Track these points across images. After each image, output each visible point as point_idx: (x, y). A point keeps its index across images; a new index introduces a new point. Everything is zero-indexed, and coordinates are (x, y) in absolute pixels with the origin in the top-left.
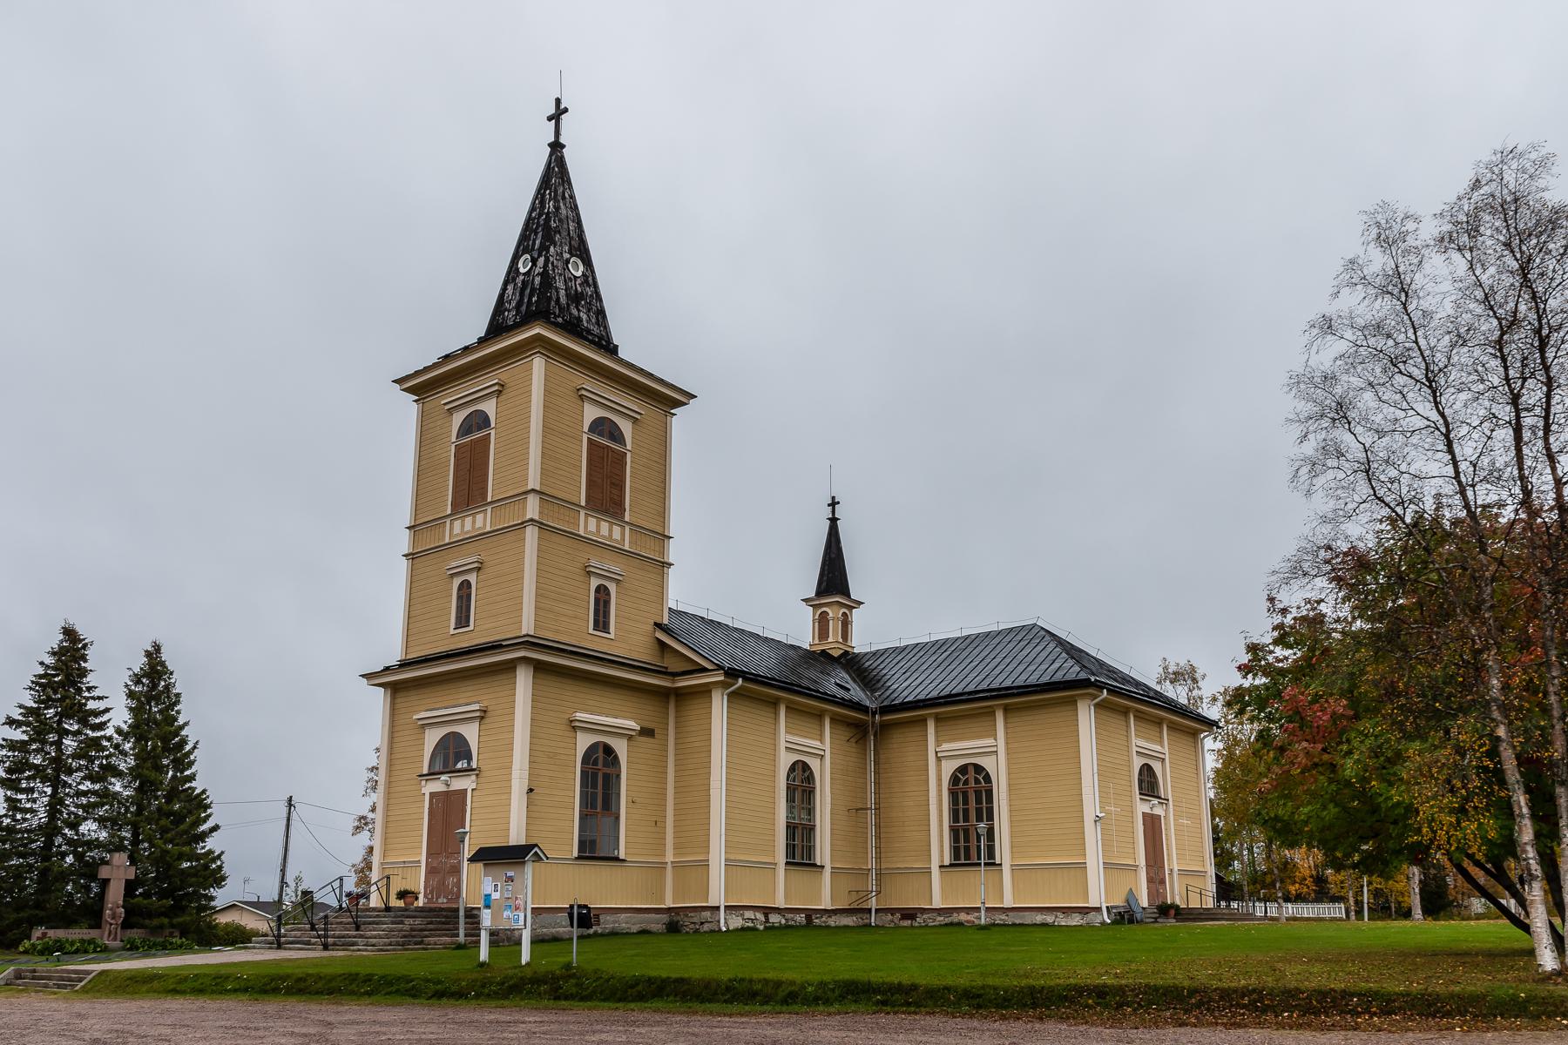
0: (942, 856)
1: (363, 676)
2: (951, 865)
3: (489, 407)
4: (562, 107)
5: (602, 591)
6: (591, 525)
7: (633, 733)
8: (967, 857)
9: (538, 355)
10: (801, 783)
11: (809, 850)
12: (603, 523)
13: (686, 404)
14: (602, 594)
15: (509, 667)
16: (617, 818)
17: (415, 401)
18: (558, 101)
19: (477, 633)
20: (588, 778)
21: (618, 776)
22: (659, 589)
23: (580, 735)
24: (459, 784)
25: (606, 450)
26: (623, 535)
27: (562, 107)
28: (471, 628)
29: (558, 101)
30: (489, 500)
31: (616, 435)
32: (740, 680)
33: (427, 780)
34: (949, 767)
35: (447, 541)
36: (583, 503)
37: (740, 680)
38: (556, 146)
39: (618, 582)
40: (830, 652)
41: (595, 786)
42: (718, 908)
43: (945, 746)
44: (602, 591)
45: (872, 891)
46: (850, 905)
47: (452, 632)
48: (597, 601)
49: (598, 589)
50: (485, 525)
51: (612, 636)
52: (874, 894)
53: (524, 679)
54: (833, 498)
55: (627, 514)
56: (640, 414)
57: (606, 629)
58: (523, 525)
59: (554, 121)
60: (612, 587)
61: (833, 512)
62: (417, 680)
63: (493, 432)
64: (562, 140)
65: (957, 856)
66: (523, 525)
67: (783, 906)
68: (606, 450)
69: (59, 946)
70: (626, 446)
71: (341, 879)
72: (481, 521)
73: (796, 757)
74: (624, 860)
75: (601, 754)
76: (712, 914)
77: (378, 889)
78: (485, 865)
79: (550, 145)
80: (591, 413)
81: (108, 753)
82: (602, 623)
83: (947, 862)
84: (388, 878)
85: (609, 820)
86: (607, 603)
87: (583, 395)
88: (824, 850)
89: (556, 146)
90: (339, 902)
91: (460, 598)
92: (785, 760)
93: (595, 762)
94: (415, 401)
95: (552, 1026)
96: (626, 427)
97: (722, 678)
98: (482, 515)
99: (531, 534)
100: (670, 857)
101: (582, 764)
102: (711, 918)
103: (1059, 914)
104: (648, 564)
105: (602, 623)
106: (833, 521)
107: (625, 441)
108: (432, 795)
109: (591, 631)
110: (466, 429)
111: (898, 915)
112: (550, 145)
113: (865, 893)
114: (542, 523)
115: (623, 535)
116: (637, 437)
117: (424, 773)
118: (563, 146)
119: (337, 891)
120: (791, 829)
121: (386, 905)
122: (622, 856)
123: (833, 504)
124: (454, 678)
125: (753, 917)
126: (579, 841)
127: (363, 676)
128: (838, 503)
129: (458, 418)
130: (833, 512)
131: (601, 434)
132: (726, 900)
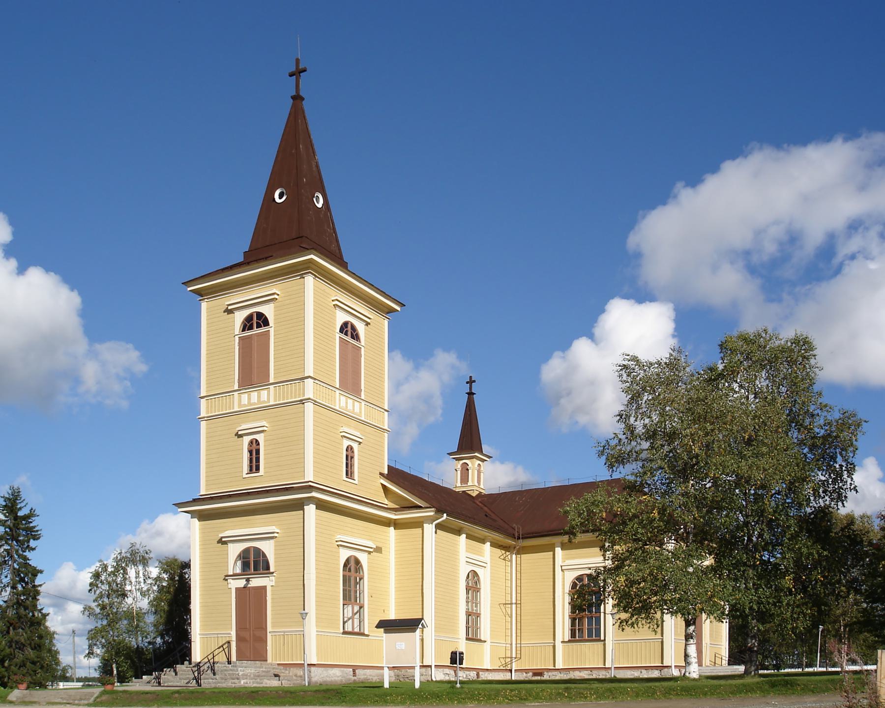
2: (569, 641)
3: (267, 310)
5: (350, 449)
7: (372, 550)
11: (477, 629)
19: (264, 478)
24: (256, 582)
27: (301, 67)
30: (271, 381)
32: (445, 515)
34: (571, 576)
36: (338, 386)
37: (445, 515)
39: (360, 443)
40: (467, 492)
42: (430, 666)
44: (350, 449)
46: (499, 667)
47: (245, 476)
54: (471, 377)
56: (370, 318)
58: (302, 402)
60: (355, 446)
61: (471, 388)
62: (208, 510)
66: (302, 402)
70: (360, 342)
72: (265, 396)
74: (368, 636)
78: (385, 630)
80: (341, 318)
82: (349, 473)
83: (566, 639)
88: (485, 632)
92: (464, 570)
96: (360, 327)
99: (309, 406)
103: (642, 670)
110: (248, 324)
111: (531, 674)
114: (315, 401)
115: (360, 408)
117: (229, 574)
118: (303, 99)
119: (226, 650)
122: (366, 633)
123: (471, 382)
124: (376, 516)
125: (449, 673)
129: (240, 317)
130: (471, 388)
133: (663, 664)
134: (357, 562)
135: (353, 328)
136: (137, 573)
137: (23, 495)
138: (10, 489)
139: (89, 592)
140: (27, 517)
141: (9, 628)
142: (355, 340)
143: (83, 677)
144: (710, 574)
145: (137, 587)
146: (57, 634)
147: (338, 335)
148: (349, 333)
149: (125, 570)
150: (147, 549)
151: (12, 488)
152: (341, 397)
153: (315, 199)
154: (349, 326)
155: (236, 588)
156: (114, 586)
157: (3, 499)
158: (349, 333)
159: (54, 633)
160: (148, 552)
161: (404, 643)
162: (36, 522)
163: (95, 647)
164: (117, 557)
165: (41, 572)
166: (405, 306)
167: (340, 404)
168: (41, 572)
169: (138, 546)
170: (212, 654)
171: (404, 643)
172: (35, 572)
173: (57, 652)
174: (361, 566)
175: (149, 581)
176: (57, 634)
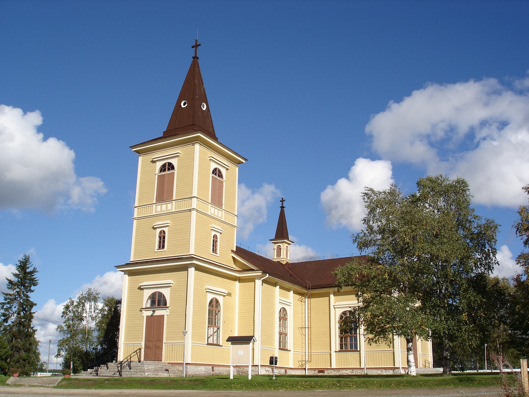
0: (336, 347)
2: (339, 351)
3: (174, 162)
5: (215, 237)
6: (212, 210)
7: (225, 294)
8: (346, 348)
10: (283, 316)
11: (285, 343)
12: (216, 210)
15: (185, 268)
23: (208, 294)
24: (158, 313)
26: (222, 214)
30: (174, 199)
31: (221, 176)
32: (268, 275)
35: (154, 214)
36: (210, 202)
37: (268, 275)
42: (258, 366)
43: (338, 303)
44: (215, 237)
47: (156, 251)
50: (172, 208)
51: (218, 255)
53: (192, 270)
55: (223, 206)
60: (218, 235)
61: (282, 204)
64: (198, 56)
65: (341, 347)
66: (190, 210)
67: (335, 367)
69: (56, 375)
70: (223, 179)
72: (170, 207)
73: (213, 296)
76: (255, 368)
80: (213, 166)
83: (338, 350)
96: (223, 171)
97: (260, 274)
99: (194, 213)
102: (255, 370)
104: (230, 226)
105: (214, 250)
106: (282, 207)
110: (163, 169)
111: (317, 371)
114: (197, 210)
116: (200, 169)
117: (143, 307)
119: (138, 354)
120: (281, 334)
122: (221, 344)
123: (283, 201)
128: (284, 201)
129: (159, 165)
130: (282, 204)
132: (261, 363)
136: (91, 306)
137: (31, 260)
138: (24, 256)
139: (62, 317)
140: (31, 273)
141: (12, 338)
143: (53, 370)
145: (90, 315)
146: (40, 342)
147: (211, 175)
148: (217, 174)
149: (84, 304)
150: (97, 292)
151: (25, 256)
153: (202, 106)
154: (217, 170)
155: (147, 316)
156: (77, 314)
157: (19, 262)
158: (217, 174)
159: (39, 342)
160: (98, 294)
162: (36, 276)
163: (62, 351)
164: (80, 297)
165: (35, 305)
166: (247, 160)
167: (211, 212)
168: (35, 305)
169: (92, 290)
172: (32, 305)
173: (39, 354)
174: (219, 304)
175: (97, 311)
176: (40, 342)
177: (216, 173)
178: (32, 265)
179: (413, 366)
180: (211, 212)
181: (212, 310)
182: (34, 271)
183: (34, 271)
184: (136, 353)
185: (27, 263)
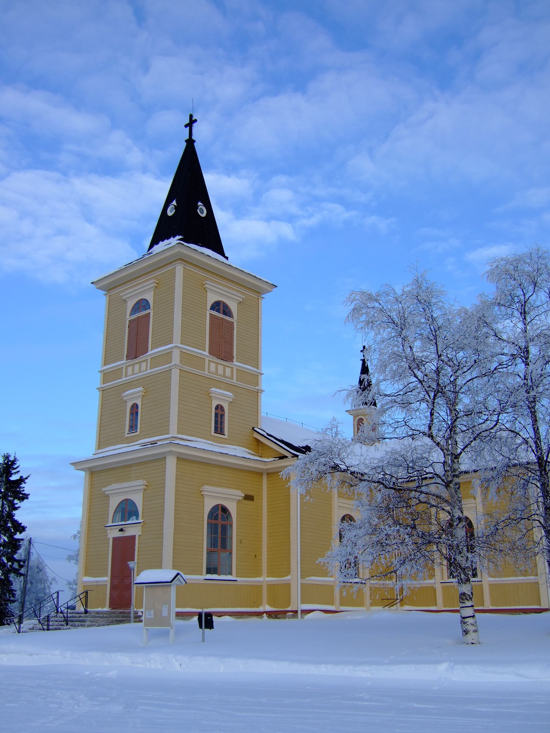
1: (72, 464)
4: (194, 119)
9: (179, 264)
13: (271, 291)
14: (219, 411)
16: (231, 553)
17: (105, 295)
18: (191, 116)
20: (212, 528)
21: (231, 526)
22: (257, 345)
25: (221, 320)
27: (194, 119)
28: (138, 433)
29: (191, 116)
31: (227, 311)
33: (111, 529)
38: (190, 142)
41: (216, 533)
45: (397, 599)
47: (127, 436)
48: (216, 415)
49: (217, 407)
51: (226, 437)
52: (398, 601)
57: (222, 433)
59: (188, 127)
63: (151, 311)
64: (194, 138)
68: (221, 320)
70: (233, 318)
71: (58, 593)
75: (220, 511)
77: (81, 599)
79: (186, 141)
81: (6, 561)
84: (87, 592)
85: (224, 555)
86: (222, 416)
87: (206, 287)
89: (190, 142)
90: (56, 607)
91: (132, 414)
93: (216, 518)
94: (105, 295)
95: (460, 721)
98: (145, 363)
100: (264, 579)
101: (208, 519)
107: (232, 315)
108: (115, 539)
109: (213, 433)
112: (186, 141)
113: (393, 601)
119: (55, 600)
121: (85, 610)
126: (207, 568)
127: (72, 464)
131: (218, 311)
133: (540, 605)
134: (224, 510)
135: (226, 306)
142: (227, 316)
144: (542, 479)
147: (209, 312)
148: (221, 310)
152: (211, 364)
153: (198, 211)
154: (221, 305)
155: (113, 538)
158: (221, 310)
161: (152, 616)
162: (27, 488)
166: (277, 287)
167: (209, 369)
170: (66, 604)
171: (152, 616)
174: (230, 514)
177: (219, 309)
178: (19, 472)
179: (471, 632)
180: (209, 369)
181: (216, 525)
182: (22, 480)
183: (22, 480)
184: (78, 598)
185: (13, 471)
